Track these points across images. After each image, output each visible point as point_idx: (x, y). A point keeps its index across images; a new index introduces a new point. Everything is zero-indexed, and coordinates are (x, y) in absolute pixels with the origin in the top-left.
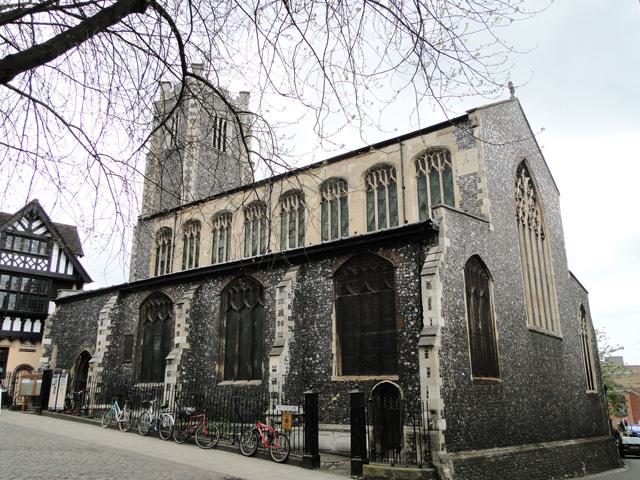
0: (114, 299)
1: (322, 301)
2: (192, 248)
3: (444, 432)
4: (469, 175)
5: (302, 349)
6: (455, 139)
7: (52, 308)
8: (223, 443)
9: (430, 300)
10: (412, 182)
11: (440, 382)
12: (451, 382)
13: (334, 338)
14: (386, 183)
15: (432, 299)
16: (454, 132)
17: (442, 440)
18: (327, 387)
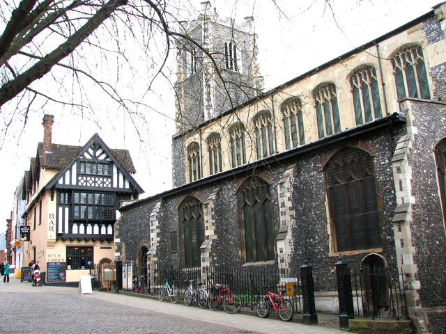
0: (159, 204)
1: (316, 191)
2: (215, 157)
3: (418, 291)
4: (440, 65)
5: (303, 234)
6: (424, 34)
7: (118, 215)
8: (244, 309)
9: (401, 182)
10: (390, 79)
11: (413, 250)
12: (425, 249)
13: (328, 221)
14: (368, 82)
15: (403, 181)
16: (422, 29)
17: (417, 297)
18: (326, 262)
